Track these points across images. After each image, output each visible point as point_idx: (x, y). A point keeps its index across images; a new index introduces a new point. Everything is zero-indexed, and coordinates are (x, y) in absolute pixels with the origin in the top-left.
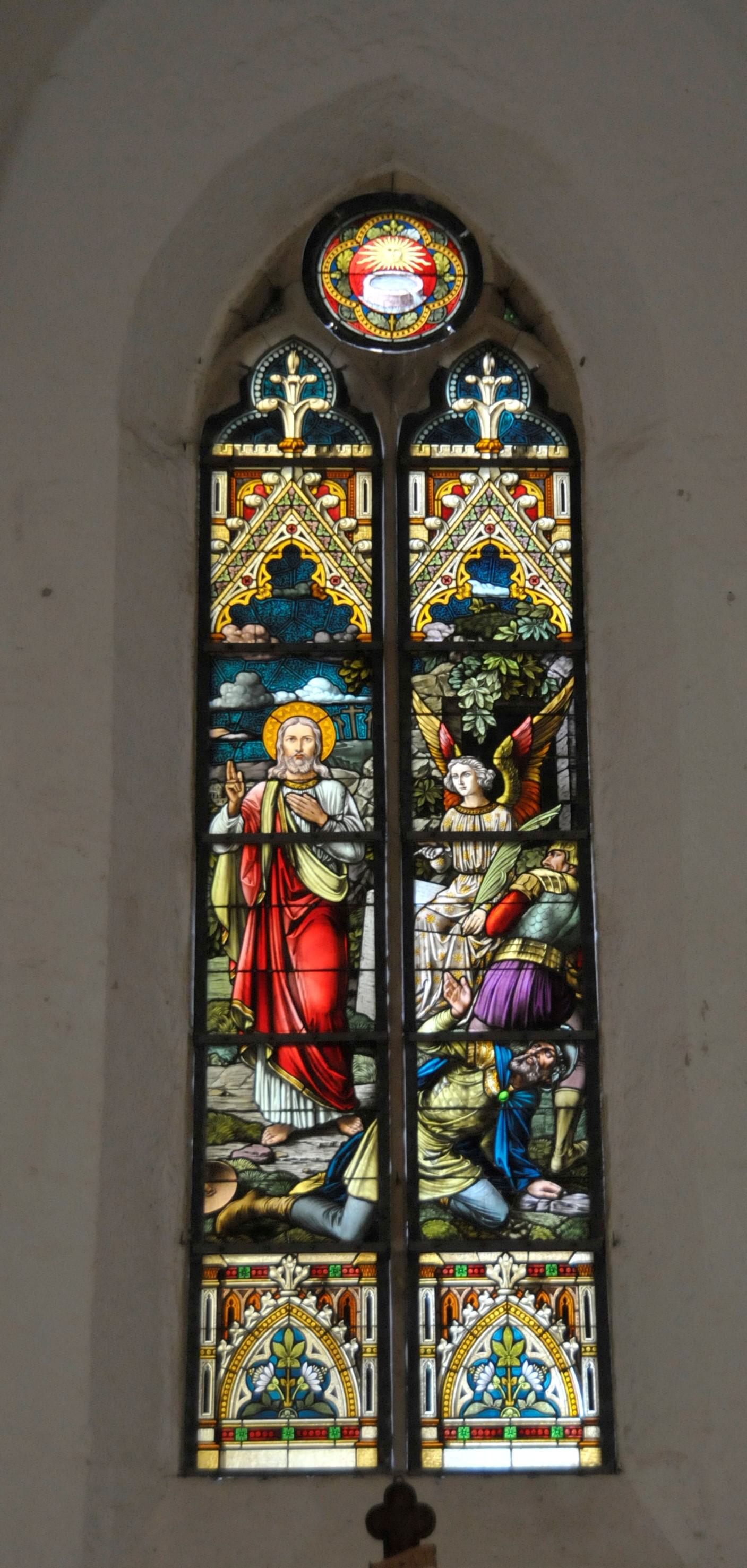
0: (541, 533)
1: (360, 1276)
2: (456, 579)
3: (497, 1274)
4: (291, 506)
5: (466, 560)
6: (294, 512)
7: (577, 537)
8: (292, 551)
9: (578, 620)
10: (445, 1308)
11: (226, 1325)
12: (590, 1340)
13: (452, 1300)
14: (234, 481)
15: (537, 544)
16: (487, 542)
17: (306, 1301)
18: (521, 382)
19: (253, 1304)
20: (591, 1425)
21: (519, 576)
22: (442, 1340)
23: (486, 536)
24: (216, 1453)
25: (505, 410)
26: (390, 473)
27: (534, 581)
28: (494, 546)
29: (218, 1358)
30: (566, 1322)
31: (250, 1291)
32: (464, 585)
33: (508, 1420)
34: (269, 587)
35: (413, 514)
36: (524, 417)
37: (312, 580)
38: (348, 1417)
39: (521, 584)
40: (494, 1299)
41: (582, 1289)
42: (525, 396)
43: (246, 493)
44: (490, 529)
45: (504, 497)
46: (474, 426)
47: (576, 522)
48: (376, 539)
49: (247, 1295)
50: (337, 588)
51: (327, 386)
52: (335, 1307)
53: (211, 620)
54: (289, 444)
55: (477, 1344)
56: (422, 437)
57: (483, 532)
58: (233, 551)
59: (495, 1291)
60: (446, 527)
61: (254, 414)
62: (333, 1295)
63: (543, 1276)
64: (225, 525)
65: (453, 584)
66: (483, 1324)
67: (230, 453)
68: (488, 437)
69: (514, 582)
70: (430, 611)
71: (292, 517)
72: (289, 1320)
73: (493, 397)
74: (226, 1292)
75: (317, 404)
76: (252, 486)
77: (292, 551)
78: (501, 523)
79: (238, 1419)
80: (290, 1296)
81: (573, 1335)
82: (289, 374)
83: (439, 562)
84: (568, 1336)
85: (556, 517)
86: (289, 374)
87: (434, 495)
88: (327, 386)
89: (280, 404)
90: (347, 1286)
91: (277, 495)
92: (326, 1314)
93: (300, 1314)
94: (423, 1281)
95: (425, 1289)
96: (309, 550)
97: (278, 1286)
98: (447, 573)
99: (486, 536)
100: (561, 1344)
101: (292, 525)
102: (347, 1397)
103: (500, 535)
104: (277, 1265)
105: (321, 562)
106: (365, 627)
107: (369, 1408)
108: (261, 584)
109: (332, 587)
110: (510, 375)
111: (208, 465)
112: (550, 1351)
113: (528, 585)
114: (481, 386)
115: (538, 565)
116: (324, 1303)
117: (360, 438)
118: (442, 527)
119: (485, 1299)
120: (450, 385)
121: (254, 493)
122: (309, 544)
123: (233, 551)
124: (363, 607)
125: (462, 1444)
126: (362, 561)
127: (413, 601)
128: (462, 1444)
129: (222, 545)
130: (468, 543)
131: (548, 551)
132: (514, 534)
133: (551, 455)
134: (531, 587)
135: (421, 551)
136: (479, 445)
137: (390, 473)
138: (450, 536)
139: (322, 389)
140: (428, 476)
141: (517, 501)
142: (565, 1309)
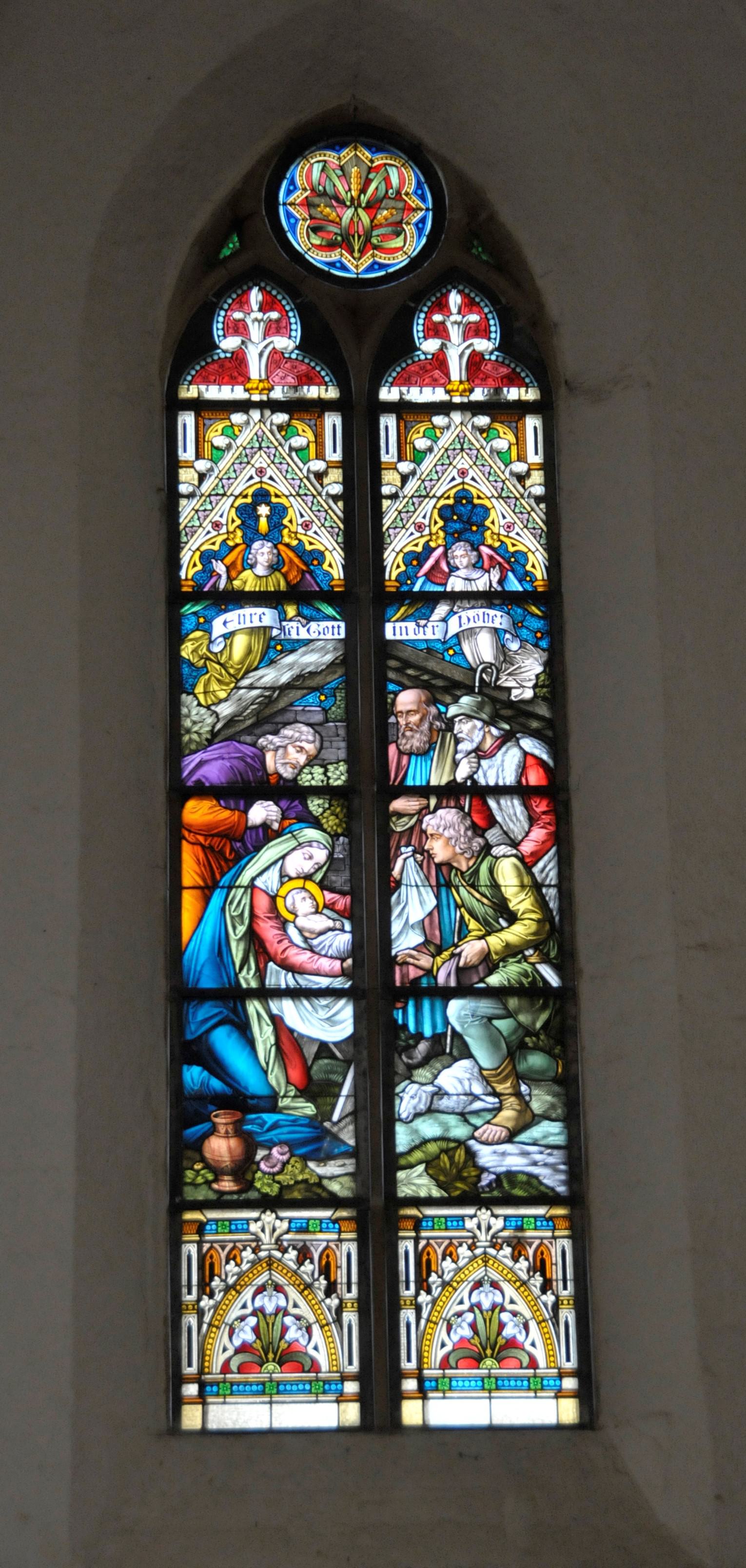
0: (312, 476)
1: (554, 1229)
2: (429, 526)
3: (475, 1227)
4: (462, 450)
5: (438, 506)
6: (465, 455)
7: (550, 482)
8: (463, 497)
9: (554, 566)
10: (207, 1263)
11: (207, 1280)
12: (565, 1293)
13: (545, 1253)
14: (201, 422)
15: (512, 486)
16: (259, 486)
17: (501, 1253)
18: (488, 320)
19: (451, 1255)
20: (193, 1383)
21: (493, 523)
22: (422, 1292)
23: (257, 479)
24: (200, 1407)
25: (274, 348)
26: (361, 417)
27: (420, 527)
28: (467, 490)
29: (201, 1313)
30: (543, 1274)
31: (230, 1245)
32: (437, 533)
33: (487, 1371)
34: (441, 534)
35: (183, 456)
36: (294, 356)
37: (282, 525)
38: (547, 1368)
39: (293, 529)
40: (472, 1251)
41: (345, 1246)
42: (493, 335)
43: (212, 434)
44: (463, 473)
45: (478, 441)
46: (243, 367)
47: (549, 467)
48: (347, 482)
49: (227, 1249)
50: (511, 535)
51: (290, 324)
52: (531, 1259)
53: (385, 568)
54: (255, 386)
55: (456, 1297)
56: (390, 379)
57: (457, 477)
58: (202, 495)
59: (474, 1244)
60: (216, 471)
61: (218, 354)
62: (528, 1248)
63: (520, 1229)
64: (396, 469)
65: (224, 530)
66: (459, 1279)
67: (195, 395)
68: (258, 378)
69: (286, 527)
70: (201, 558)
71: (463, 461)
72: (486, 1270)
73: (261, 335)
74: (206, 1246)
75: (482, 345)
76: (220, 427)
77: (463, 497)
78: (474, 467)
79: (221, 1373)
80: (485, 1247)
81: (551, 1288)
82: (451, 314)
83: (209, 507)
84: (546, 1287)
85: (327, 459)
86: (451, 314)
87: (204, 436)
88: (290, 324)
89: (243, 342)
90: (542, 1238)
91: (244, 438)
92: (523, 1264)
93: (280, 1268)
94: (186, 1238)
95: (188, 1245)
96: (279, 494)
97: (258, 1240)
98: (420, 520)
99: (257, 479)
100: (323, 1301)
101: (261, 468)
102: (331, 1348)
103: (473, 479)
104: (256, 1220)
105: (292, 506)
106: (337, 573)
107: (350, 1363)
108: (434, 530)
109: (303, 532)
110: (479, 313)
111: (175, 406)
112: (312, 1307)
113: (300, 530)
114: (448, 324)
115: (513, 511)
116: (520, 1255)
117: (327, 379)
118: (211, 470)
119: (248, 1255)
120: (218, 322)
121: (424, 436)
122: (482, 488)
123: (404, 497)
124: (334, 553)
125: (314, 1399)
126: (534, 505)
127: (183, 548)
128: (441, 1395)
129: (191, 489)
130: (238, 487)
131: (320, 494)
132: (488, 479)
133: (523, 398)
134: (506, 534)
135: (191, 496)
136: (249, 386)
137: (361, 417)
138: (221, 479)
139: (286, 328)
140: (197, 416)
141: (288, 443)
142: (543, 1262)
